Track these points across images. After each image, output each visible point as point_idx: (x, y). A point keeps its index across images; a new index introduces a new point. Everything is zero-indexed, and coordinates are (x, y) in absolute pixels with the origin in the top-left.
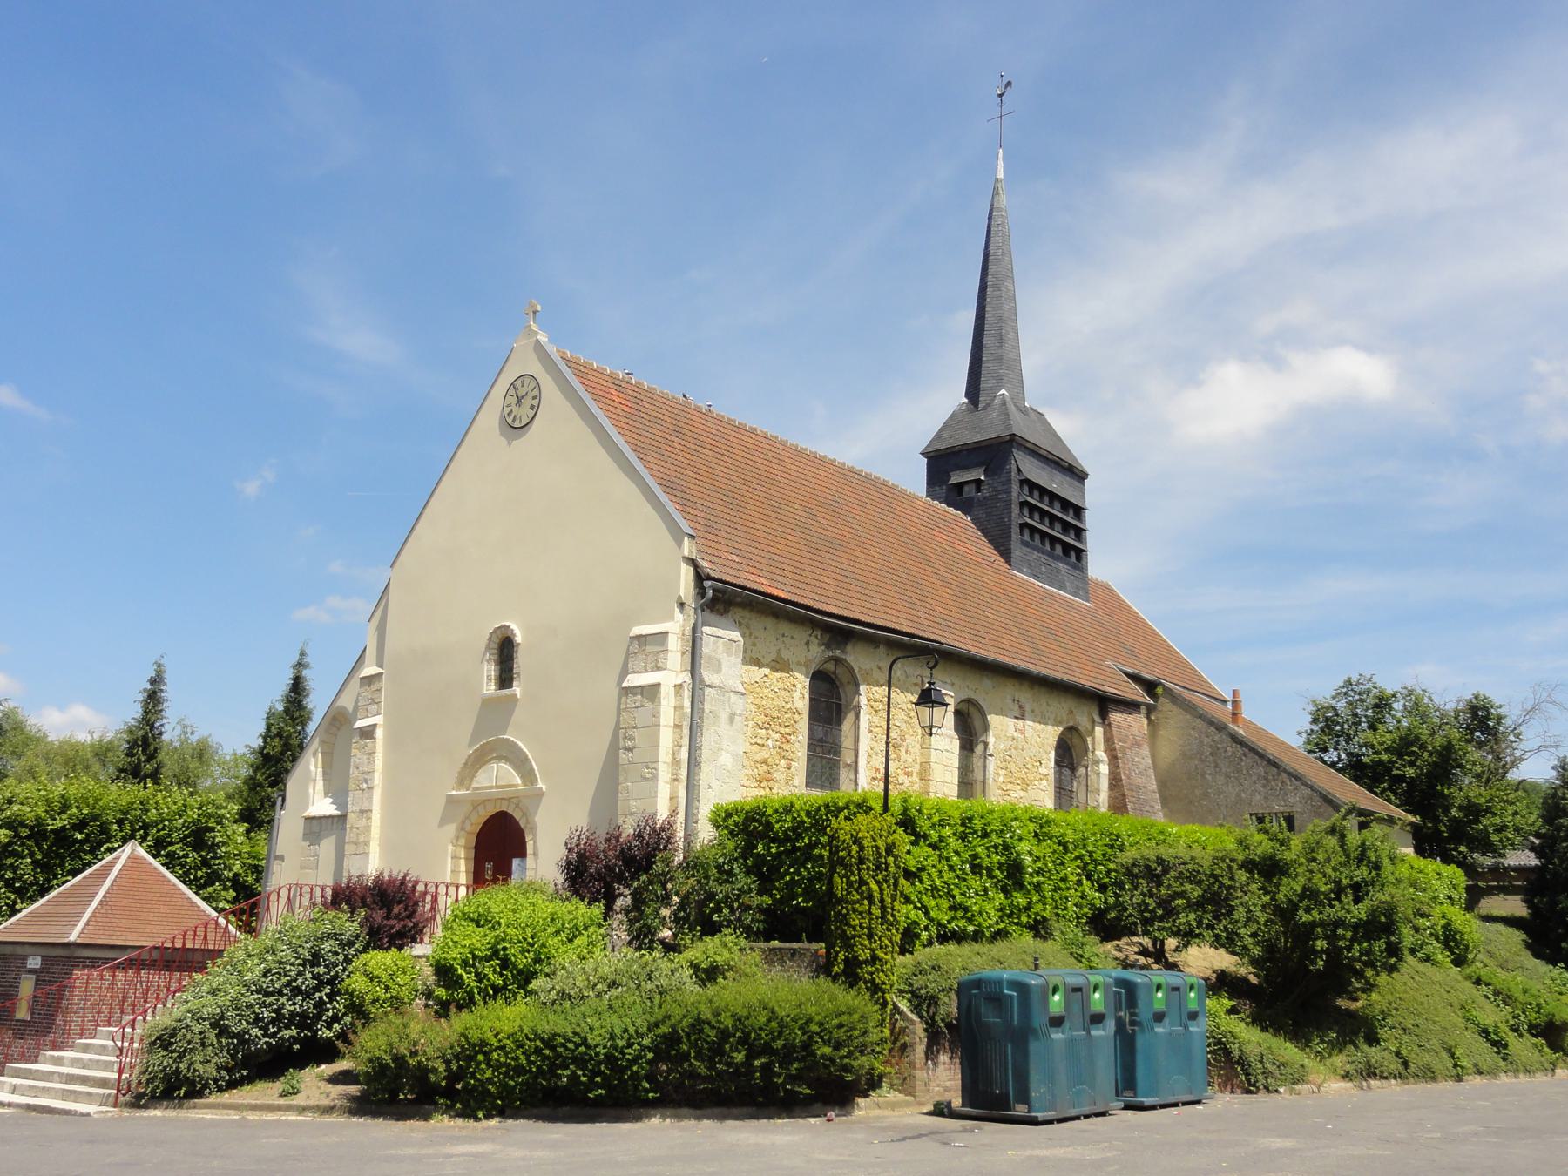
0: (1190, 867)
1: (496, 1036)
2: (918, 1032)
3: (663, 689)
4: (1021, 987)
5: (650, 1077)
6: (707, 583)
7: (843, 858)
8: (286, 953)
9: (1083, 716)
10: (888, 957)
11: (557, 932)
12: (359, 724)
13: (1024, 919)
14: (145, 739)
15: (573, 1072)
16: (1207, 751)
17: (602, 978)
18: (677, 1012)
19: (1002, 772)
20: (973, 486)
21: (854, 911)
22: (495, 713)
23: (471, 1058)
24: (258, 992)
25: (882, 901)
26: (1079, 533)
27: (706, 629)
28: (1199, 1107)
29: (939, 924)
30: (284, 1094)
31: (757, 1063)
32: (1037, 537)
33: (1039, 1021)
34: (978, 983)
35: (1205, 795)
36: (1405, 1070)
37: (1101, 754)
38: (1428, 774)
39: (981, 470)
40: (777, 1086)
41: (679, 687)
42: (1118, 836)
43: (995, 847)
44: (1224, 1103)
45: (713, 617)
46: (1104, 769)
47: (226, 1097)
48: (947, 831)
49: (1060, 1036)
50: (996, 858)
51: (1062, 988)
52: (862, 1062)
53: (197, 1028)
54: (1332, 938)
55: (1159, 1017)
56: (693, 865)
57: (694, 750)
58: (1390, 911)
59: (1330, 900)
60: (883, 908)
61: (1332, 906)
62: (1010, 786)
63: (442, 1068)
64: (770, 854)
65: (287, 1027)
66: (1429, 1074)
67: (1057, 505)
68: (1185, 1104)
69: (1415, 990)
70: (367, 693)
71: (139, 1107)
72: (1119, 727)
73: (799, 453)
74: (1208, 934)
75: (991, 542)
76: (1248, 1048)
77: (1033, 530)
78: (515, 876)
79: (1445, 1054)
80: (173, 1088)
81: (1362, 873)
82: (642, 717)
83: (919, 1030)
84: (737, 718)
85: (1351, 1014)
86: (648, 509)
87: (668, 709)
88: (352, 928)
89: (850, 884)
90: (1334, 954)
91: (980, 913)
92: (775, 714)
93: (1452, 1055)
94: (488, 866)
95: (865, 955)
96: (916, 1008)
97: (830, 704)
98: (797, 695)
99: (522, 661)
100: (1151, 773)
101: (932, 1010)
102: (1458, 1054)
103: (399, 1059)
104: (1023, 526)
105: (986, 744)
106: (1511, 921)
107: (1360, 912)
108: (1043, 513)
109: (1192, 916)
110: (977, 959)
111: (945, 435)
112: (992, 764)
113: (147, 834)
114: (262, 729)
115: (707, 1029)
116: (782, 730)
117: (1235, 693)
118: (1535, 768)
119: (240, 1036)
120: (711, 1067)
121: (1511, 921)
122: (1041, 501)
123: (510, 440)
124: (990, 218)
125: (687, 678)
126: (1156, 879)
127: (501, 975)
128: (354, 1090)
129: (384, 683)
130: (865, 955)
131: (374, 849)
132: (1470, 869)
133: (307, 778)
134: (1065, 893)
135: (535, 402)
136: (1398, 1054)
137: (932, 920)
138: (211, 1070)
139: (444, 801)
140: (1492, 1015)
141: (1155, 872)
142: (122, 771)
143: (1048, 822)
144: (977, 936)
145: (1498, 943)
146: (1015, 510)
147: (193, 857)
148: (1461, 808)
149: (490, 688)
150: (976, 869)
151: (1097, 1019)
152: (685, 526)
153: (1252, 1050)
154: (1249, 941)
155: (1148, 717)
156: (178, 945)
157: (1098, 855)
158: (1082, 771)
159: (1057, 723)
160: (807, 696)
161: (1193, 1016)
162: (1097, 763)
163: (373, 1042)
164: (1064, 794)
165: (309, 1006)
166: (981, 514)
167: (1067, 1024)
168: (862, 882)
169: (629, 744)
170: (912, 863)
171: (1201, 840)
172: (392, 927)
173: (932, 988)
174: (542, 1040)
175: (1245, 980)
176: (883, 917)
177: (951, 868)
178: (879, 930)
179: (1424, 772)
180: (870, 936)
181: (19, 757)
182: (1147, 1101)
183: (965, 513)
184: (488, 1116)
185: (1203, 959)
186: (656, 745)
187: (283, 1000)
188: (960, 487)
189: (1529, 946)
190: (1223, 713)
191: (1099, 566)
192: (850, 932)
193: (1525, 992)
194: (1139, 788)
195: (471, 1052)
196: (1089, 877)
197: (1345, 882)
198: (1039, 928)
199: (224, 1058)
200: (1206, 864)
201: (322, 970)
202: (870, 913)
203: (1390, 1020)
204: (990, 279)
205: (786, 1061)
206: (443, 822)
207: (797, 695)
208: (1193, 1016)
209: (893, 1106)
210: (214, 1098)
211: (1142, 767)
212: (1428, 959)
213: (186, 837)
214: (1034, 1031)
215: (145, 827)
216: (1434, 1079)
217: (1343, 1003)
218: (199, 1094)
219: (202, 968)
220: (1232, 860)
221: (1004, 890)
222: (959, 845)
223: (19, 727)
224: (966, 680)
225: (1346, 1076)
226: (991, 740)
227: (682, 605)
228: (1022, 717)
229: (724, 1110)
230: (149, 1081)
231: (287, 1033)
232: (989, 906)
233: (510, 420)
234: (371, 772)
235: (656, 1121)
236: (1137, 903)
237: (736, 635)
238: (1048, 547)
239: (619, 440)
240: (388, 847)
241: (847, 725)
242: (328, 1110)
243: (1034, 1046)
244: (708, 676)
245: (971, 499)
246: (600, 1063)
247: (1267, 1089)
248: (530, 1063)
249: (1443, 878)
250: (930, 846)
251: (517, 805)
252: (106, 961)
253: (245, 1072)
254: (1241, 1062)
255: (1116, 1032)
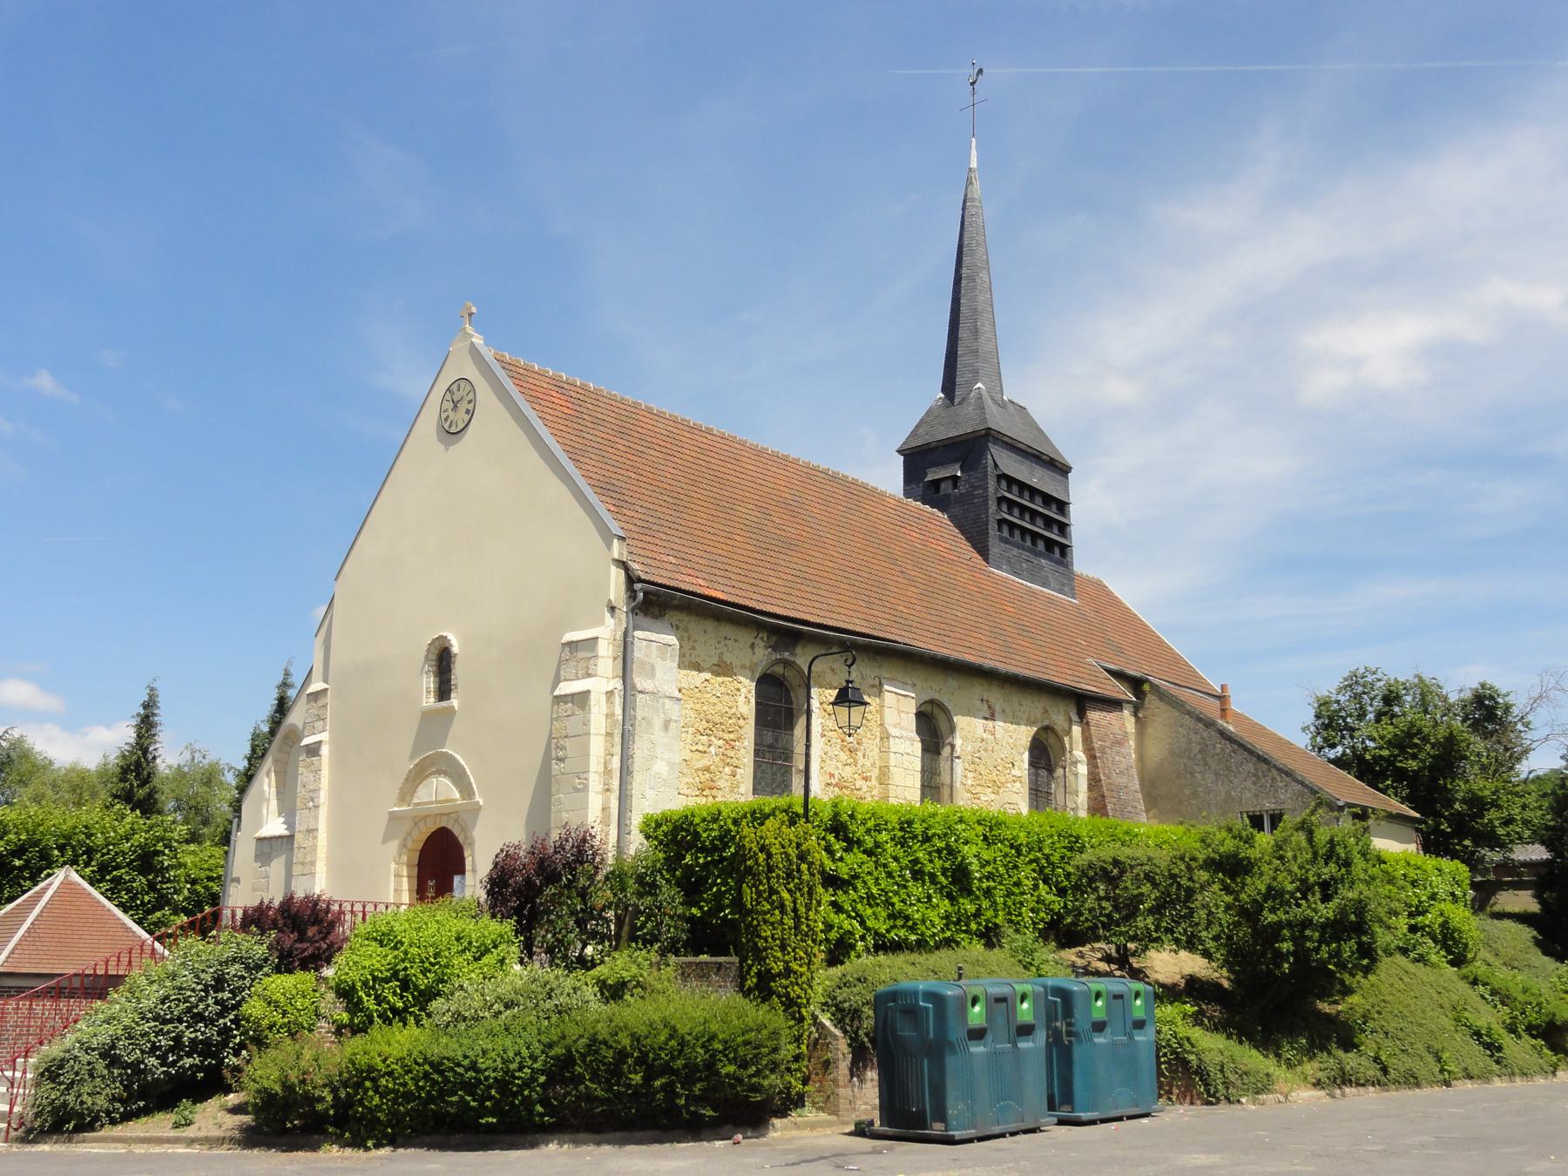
0: (1147, 868)
1: (384, 1061)
2: (842, 1047)
3: (593, 696)
4: (937, 998)
5: (544, 1102)
6: (638, 586)
7: (751, 868)
8: (187, 978)
9: (1059, 715)
10: (804, 969)
11: (463, 951)
12: (306, 741)
13: (974, 926)
14: (138, 764)
15: (462, 1098)
16: (1196, 748)
17: (504, 1000)
18: (573, 1031)
19: (970, 775)
20: (950, 483)
21: (765, 922)
22: (435, 726)
23: (359, 1085)
24: (155, 1019)
25: (795, 910)
26: (1063, 528)
27: (638, 634)
28: (1145, 1121)
29: (877, 933)
30: (177, 1126)
31: (657, 1083)
32: (1017, 533)
33: (956, 1033)
34: (893, 996)
35: (1195, 794)
36: (1384, 1076)
37: (1079, 754)
38: (1432, 768)
39: (958, 466)
40: (680, 1108)
41: (610, 694)
42: (1078, 838)
43: (939, 851)
44: (1178, 1116)
45: (647, 621)
46: (1083, 769)
47: (119, 1130)
48: (884, 836)
49: (981, 1049)
50: (938, 863)
51: (982, 998)
52: (772, 1080)
53: (85, 1058)
54: (1299, 940)
55: (1099, 1027)
56: (617, 878)
57: (626, 759)
58: (1360, 907)
59: (1297, 899)
60: (797, 918)
61: (1298, 906)
62: (979, 789)
63: (329, 1098)
64: (698, 864)
65: (189, 1055)
66: (1412, 1080)
67: (1038, 500)
68: (1130, 1118)
69: (1398, 991)
70: (314, 708)
71: (29, 1142)
72: (1098, 726)
73: (759, 453)
74: (1167, 938)
75: (968, 539)
76: (1207, 1057)
77: (1012, 526)
78: (456, 893)
79: (1430, 1059)
80: (61, 1122)
81: (1329, 870)
82: (572, 726)
83: (842, 1046)
84: (673, 725)
85: (1330, 1019)
86: (579, 511)
87: (599, 717)
88: (261, 951)
89: (759, 893)
90: (1301, 955)
91: (923, 921)
92: (717, 719)
93: (1439, 1060)
94: (431, 883)
95: (778, 967)
96: (839, 1023)
97: (779, 709)
98: (741, 699)
99: (460, 673)
100: (1134, 772)
101: (856, 1023)
102: (1445, 1056)
103: (288, 1087)
104: (1001, 522)
105: (953, 747)
106: (1523, 918)
107: (1327, 911)
108: (1023, 509)
109: (1150, 920)
110: (910, 970)
111: (921, 431)
112: (959, 766)
113: (90, 859)
114: (247, 751)
115: (604, 1051)
116: (726, 736)
117: (1223, 687)
118: (1541, 761)
119: (135, 1065)
120: (609, 1090)
121: (1523, 918)
122: (1021, 496)
123: (447, 446)
124: (964, 209)
125: (618, 684)
126: (1112, 881)
127: (402, 997)
128: (247, 1119)
129: (329, 699)
130: (778, 967)
131: (321, 869)
132: (1472, 862)
133: (262, 799)
134: (1018, 899)
135: (470, 407)
136: (1376, 1059)
137: (868, 929)
138: (101, 1102)
139: (386, 818)
140: (1489, 1017)
141: (1111, 873)
142: (116, 796)
143: (999, 824)
144: (921, 945)
145: (1506, 944)
146: (993, 506)
147: (140, 881)
148: (1464, 801)
149: (430, 701)
150: (918, 875)
151: (1026, 1030)
152: (615, 527)
153: (1212, 1060)
154: (1211, 945)
155: (1135, 714)
156: (100, 972)
157: (1055, 858)
158: (1059, 772)
159: (1030, 723)
160: (753, 701)
161: (1139, 1025)
162: (1075, 763)
163: (264, 1071)
164: (1039, 796)
165: (212, 1033)
166: (957, 510)
167: (989, 1037)
168: (772, 891)
169: (561, 754)
170: (845, 870)
171: (1154, 837)
172: (304, 950)
173: (856, 1001)
174: (431, 1064)
175: (1218, 986)
176: (797, 927)
177: (890, 875)
178: (793, 940)
179: (1427, 762)
180: (783, 948)
181: (26, 785)
182: (1085, 1116)
183: (942, 511)
184: (377, 1146)
185: (1169, 963)
186: (586, 754)
187: (182, 1027)
188: (936, 483)
189: (1538, 943)
190: (1211, 708)
191: (1082, 563)
192: (762, 944)
193: (1525, 991)
194: (1119, 788)
195: (362, 1077)
196: (1045, 882)
197: (1312, 880)
198: (990, 936)
199: (118, 1089)
200: (1164, 865)
201: (227, 995)
202: (782, 923)
203: (1371, 1024)
204: (964, 271)
205: (688, 1082)
206: (385, 840)
207: (741, 699)
208: (1139, 1025)
209: (813, 1126)
210: (109, 1131)
211: (1123, 766)
212: (1421, 959)
213: (132, 861)
214: (951, 1045)
215: (90, 852)
216: (1418, 1085)
217: (1324, 1007)
218: (90, 1127)
219: (102, 996)
220: (1194, 859)
221: (950, 897)
222: (900, 853)
223: (26, 755)
224: (950, 680)
225: (1318, 1084)
226: (958, 742)
227: (612, 609)
228: (992, 717)
229: (626, 1134)
230: (37, 1115)
231: (188, 1062)
232: (933, 913)
233: (446, 426)
234: (317, 790)
235: (552, 1147)
236: (1096, 905)
237: (672, 639)
238: (1029, 543)
239: (551, 441)
240: (335, 869)
241: (799, 730)
242: (220, 1141)
243: (951, 1061)
244: (640, 682)
245: (947, 496)
246: (490, 1087)
247: (1227, 1099)
248: (419, 1088)
249: (1447, 874)
250: (864, 852)
251: (456, 820)
252: (20, 990)
253: (142, 1104)
254: (1201, 1072)
255: (1049, 1046)
